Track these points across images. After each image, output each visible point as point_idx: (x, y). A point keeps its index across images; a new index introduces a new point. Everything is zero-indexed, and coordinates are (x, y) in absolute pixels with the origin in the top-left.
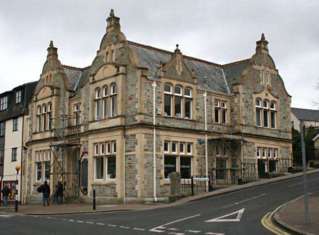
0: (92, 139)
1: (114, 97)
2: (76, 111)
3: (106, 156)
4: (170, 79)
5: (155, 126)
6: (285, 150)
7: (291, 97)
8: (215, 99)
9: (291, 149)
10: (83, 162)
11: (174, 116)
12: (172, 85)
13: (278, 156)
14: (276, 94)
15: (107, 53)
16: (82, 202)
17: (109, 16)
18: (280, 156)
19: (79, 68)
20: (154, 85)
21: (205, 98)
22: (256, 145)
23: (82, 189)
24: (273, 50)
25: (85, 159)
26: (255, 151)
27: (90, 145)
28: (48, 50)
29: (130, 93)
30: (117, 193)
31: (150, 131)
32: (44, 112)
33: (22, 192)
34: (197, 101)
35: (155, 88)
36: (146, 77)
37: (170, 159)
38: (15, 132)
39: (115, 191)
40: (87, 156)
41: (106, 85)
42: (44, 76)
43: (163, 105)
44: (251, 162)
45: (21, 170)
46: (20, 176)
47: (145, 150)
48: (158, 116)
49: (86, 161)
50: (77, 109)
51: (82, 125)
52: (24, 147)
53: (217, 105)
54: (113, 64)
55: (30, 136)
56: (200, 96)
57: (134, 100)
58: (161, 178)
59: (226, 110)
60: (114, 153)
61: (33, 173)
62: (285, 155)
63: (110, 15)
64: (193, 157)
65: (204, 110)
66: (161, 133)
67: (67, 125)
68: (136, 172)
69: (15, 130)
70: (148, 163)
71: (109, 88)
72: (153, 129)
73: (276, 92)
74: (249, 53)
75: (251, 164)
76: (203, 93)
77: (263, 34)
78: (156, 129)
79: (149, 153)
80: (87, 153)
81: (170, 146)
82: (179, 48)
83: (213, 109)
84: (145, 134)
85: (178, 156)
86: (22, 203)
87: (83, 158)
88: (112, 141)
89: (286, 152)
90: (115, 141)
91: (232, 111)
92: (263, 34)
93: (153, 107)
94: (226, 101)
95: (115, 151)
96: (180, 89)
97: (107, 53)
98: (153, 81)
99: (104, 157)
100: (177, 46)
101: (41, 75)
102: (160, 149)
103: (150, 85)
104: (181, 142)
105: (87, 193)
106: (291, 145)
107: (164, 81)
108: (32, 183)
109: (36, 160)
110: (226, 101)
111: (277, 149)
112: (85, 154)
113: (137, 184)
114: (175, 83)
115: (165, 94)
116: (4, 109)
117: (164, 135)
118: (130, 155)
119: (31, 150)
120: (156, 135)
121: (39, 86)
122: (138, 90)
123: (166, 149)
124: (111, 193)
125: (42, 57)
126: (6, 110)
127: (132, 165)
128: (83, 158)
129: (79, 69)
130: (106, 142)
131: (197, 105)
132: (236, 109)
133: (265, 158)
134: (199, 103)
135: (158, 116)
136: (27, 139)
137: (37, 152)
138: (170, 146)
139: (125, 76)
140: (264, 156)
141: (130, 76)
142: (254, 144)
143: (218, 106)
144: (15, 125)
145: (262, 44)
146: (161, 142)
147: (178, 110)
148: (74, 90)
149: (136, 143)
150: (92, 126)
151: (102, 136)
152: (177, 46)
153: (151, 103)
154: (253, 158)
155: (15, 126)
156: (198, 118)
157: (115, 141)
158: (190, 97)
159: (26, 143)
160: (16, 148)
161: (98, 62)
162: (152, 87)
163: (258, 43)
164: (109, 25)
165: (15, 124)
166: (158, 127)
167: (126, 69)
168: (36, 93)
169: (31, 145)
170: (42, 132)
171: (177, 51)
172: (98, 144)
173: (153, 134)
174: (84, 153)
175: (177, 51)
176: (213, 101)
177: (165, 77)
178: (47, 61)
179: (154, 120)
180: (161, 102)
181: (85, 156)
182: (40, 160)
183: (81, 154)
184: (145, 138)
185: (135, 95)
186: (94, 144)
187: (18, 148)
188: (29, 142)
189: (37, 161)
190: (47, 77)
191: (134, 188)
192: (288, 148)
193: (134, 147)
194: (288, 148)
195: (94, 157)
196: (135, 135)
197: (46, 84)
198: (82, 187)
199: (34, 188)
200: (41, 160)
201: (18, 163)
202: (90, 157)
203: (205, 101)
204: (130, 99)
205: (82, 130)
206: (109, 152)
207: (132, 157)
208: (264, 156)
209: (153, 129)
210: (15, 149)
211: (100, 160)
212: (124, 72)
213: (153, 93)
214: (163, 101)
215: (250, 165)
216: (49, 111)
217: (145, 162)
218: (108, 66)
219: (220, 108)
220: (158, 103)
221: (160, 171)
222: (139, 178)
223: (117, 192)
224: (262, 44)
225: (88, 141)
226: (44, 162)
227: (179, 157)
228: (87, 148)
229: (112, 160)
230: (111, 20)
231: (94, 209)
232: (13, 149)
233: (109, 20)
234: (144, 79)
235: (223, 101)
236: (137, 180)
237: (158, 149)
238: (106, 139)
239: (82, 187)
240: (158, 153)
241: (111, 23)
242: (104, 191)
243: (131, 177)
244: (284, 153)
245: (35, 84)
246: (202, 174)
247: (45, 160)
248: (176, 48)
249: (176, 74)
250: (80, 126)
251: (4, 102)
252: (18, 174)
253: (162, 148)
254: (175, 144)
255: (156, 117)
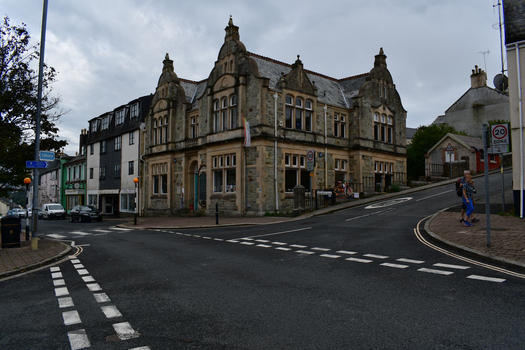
0: (210, 152)
1: (166, 127)
2: (193, 123)
3: (225, 169)
4: (292, 90)
5: (277, 138)
6: (400, 165)
7: (406, 112)
8: (335, 113)
9: (405, 164)
10: (201, 175)
11: (305, 130)
12: (293, 97)
13: (395, 169)
14: (393, 109)
15: (226, 64)
16: (200, 215)
17: (228, 26)
18: (395, 171)
19: (194, 82)
20: (276, 96)
21: (326, 111)
22: (374, 159)
23: (201, 202)
24: (391, 65)
25: (203, 172)
26: (372, 165)
27: (209, 158)
28: (163, 62)
29: (250, 104)
30: (237, 207)
31: (272, 144)
32: (160, 126)
33: (140, 205)
34: (318, 114)
35: (276, 99)
36: (267, 87)
37: (290, 174)
38: (131, 145)
39: (235, 204)
40: (206, 169)
41: (225, 97)
42: (160, 89)
43: (284, 117)
44: (369, 176)
45: (140, 183)
46: (138, 188)
47: (267, 163)
48: (279, 127)
49: (204, 174)
50: (194, 122)
51: (199, 137)
52: (141, 160)
53: (336, 119)
54: (232, 75)
55: (146, 149)
56: (320, 108)
57: (254, 112)
58: (282, 192)
59: (345, 123)
60: (233, 166)
61: (150, 186)
62: (400, 170)
63: (229, 24)
64: (346, 173)
65: (324, 123)
66: (283, 145)
67: (184, 138)
68: (257, 185)
69: (131, 144)
70: (269, 176)
71: (228, 100)
72: (274, 141)
73: (393, 106)
74: (367, 67)
75: (370, 178)
76: (323, 106)
77: (381, 49)
78: (277, 141)
79: (270, 166)
80: (205, 166)
81: (290, 160)
82: (300, 59)
83: (333, 122)
84: (266, 146)
85: (298, 169)
86: (140, 215)
87: (201, 171)
88: (232, 154)
89: (401, 167)
90: (235, 153)
91: (350, 125)
92: (381, 49)
93: (274, 118)
94: (345, 115)
95: (235, 164)
96: (301, 101)
97: (226, 64)
98: (275, 92)
99: (223, 170)
100: (298, 56)
101: (157, 88)
102: (281, 162)
103: (272, 96)
104: (342, 160)
105: (206, 206)
106: (405, 160)
107: (286, 91)
108: (150, 196)
109: (153, 173)
110: (345, 115)
111: (393, 164)
112: (203, 167)
113: (258, 198)
114: (296, 94)
115: (286, 106)
116: (120, 123)
117: (286, 148)
118: (251, 168)
119: (148, 163)
120: (277, 147)
121: (155, 98)
122: (260, 101)
123: (287, 163)
124: (230, 207)
125: (159, 70)
126: (122, 123)
127: (253, 178)
128: (201, 171)
129: (194, 83)
130: (225, 155)
131: (318, 118)
132: (355, 123)
133: (381, 172)
134: (320, 116)
135: (279, 127)
136: (145, 152)
137: (153, 165)
138: (290, 160)
139: (245, 87)
140: (380, 170)
141: (250, 88)
142: (371, 158)
143: (338, 120)
144: (92, 150)
145: (380, 59)
146: (283, 155)
147: (298, 121)
148: (191, 103)
149: (258, 156)
150: (211, 139)
151: (221, 149)
152: (298, 56)
153: (272, 115)
154: (371, 172)
155: (131, 140)
156: (318, 131)
157: (235, 153)
158: (311, 109)
159: (142, 157)
160: (133, 161)
161: (215, 74)
162: (274, 98)
163: (376, 57)
164: (228, 34)
165: (131, 137)
166: (280, 140)
167: (246, 79)
168: (152, 106)
169: (148, 158)
170: (159, 145)
171: (298, 63)
172: (223, 156)
173: (274, 147)
174: (202, 166)
175: (298, 63)
176: (333, 114)
177: (286, 88)
178: (162, 75)
179: (276, 132)
180: (282, 114)
181: (203, 169)
182: (157, 173)
183: (199, 167)
184: (266, 150)
185: (256, 107)
186: (213, 157)
187: (134, 161)
188: (146, 155)
189: (154, 174)
190: (163, 90)
191: (255, 202)
192: (403, 162)
193: (255, 160)
194: (403, 162)
195: (212, 170)
196: (256, 148)
197: (161, 97)
198: (200, 201)
199: (152, 201)
200: (158, 173)
201: (135, 177)
202: (208, 170)
203: (326, 114)
204: (251, 110)
205: (200, 142)
206: (228, 165)
207: (253, 170)
208: (380, 170)
209: (274, 141)
210: (131, 163)
211: (218, 174)
212: (244, 83)
213: (274, 105)
214: (284, 112)
215: (368, 179)
216: (165, 124)
217: (267, 176)
218: (227, 76)
219: (339, 122)
220: (280, 115)
221: (281, 184)
222: (260, 192)
223: (237, 205)
224: (380, 59)
225: (206, 154)
226: (161, 175)
227: (300, 170)
228: (205, 162)
229: (231, 173)
230: (230, 30)
231: (217, 223)
232: (130, 162)
233: (227, 29)
234: (265, 90)
235: (342, 114)
236: (258, 194)
237: (280, 162)
238: (226, 152)
239: (200, 201)
240: (279, 166)
241: (230, 32)
242: (223, 204)
243: (252, 191)
244: (399, 168)
245: (152, 96)
246: (321, 188)
247: (162, 173)
248: (297, 59)
249: (298, 86)
250: (197, 138)
251: (118, 142)
252: (136, 187)
253: (283, 161)
254: (296, 157)
255: (277, 129)
